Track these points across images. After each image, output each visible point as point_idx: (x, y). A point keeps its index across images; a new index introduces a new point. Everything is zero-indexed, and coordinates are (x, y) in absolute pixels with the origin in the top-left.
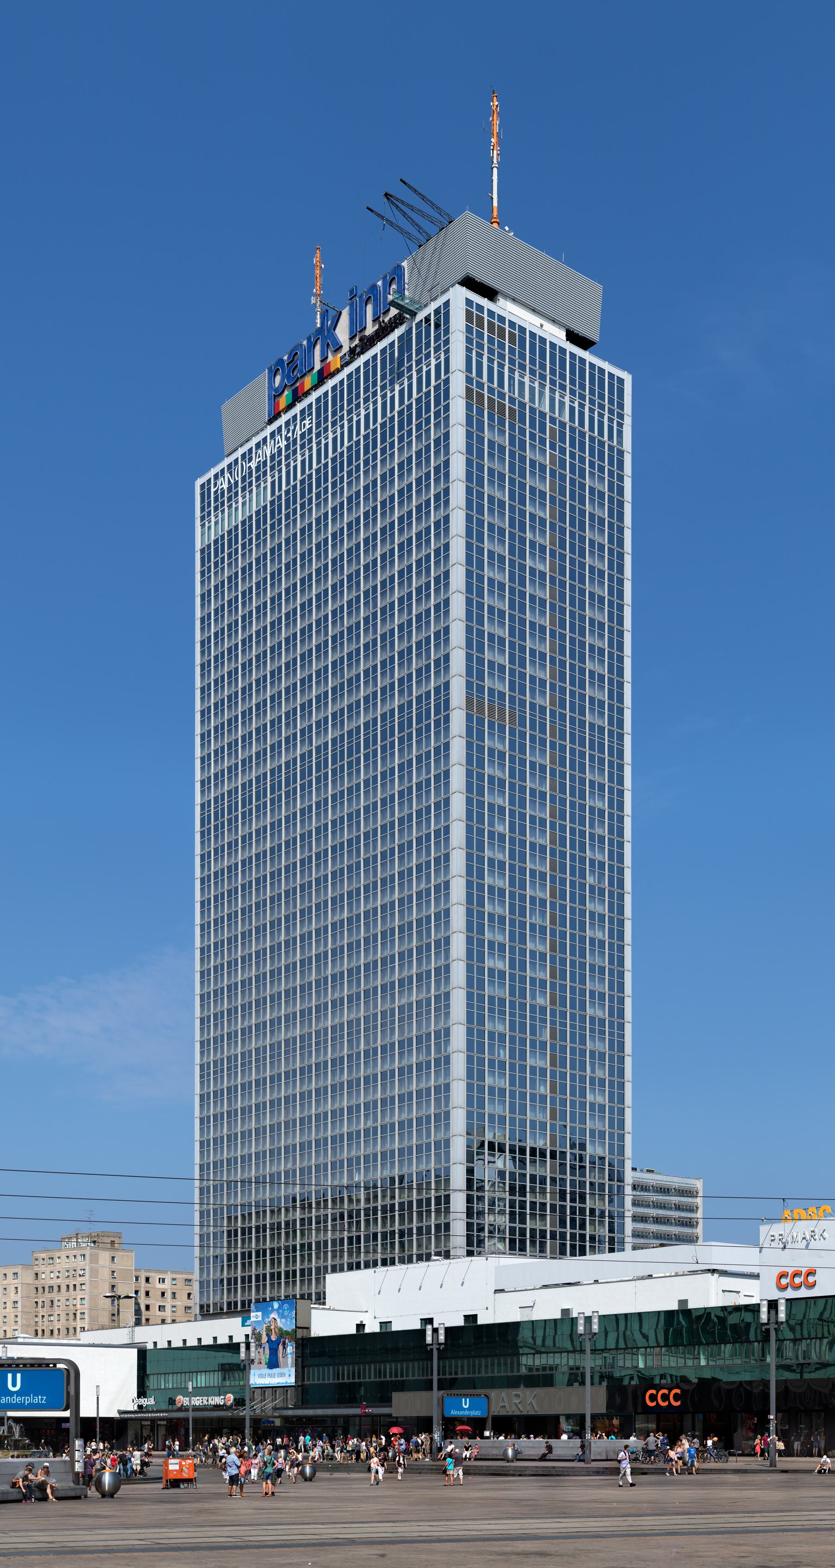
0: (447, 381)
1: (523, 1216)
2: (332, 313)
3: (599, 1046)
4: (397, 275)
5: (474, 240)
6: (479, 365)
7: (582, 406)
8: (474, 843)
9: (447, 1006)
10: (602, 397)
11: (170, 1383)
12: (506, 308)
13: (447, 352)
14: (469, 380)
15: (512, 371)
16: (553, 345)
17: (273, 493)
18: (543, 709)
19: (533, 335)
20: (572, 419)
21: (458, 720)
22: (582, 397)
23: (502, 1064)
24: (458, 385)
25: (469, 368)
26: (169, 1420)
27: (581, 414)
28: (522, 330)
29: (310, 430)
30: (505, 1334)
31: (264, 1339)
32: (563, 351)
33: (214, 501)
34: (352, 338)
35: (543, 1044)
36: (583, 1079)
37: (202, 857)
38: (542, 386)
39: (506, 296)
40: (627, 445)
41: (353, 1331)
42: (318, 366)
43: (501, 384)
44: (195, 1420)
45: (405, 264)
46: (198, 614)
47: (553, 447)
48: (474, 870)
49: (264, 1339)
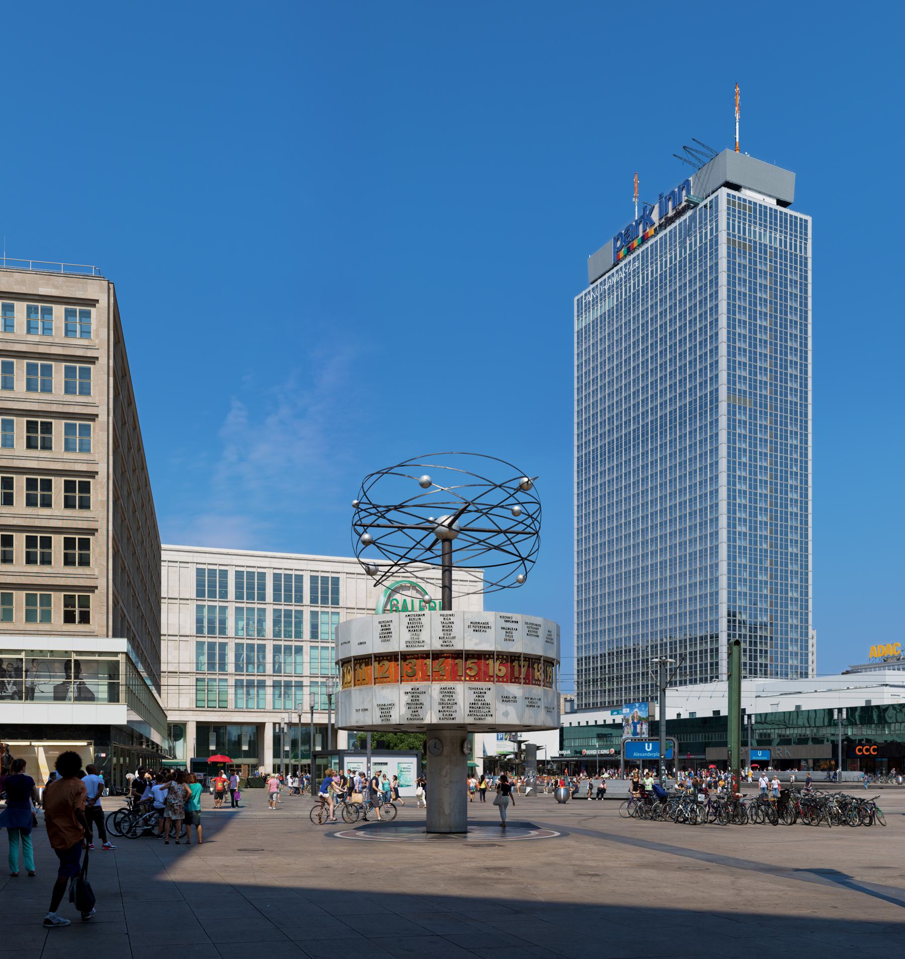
0: (717, 236)
1: (756, 657)
2: (649, 207)
3: (795, 568)
4: (686, 185)
5: (734, 163)
6: (734, 225)
7: (786, 237)
8: (731, 468)
9: (717, 552)
10: (796, 231)
11: (577, 743)
12: (746, 194)
13: (717, 221)
14: (729, 234)
15: (750, 226)
16: (771, 209)
17: (617, 300)
18: (766, 397)
19: (760, 205)
20: (781, 245)
21: (723, 408)
22: (786, 233)
23: (745, 580)
24: (723, 237)
25: (728, 228)
26: (577, 761)
27: (786, 242)
28: (755, 204)
29: (638, 268)
30: (882, 710)
31: (631, 722)
32: (776, 211)
33: (584, 308)
34: (660, 219)
35: (766, 569)
36: (787, 585)
37: (578, 483)
38: (765, 231)
39: (745, 188)
40: (809, 254)
41: (675, 718)
42: (641, 235)
43: (744, 233)
44: (600, 761)
45: (691, 179)
46: (576, 363)
47: (771, 261)
48: (731, 482)
49: (631, 722)
